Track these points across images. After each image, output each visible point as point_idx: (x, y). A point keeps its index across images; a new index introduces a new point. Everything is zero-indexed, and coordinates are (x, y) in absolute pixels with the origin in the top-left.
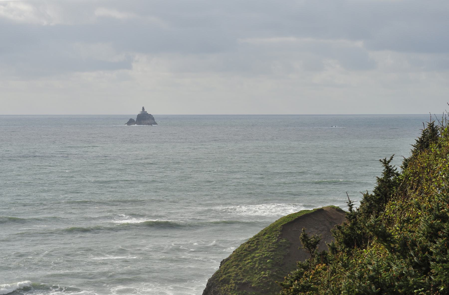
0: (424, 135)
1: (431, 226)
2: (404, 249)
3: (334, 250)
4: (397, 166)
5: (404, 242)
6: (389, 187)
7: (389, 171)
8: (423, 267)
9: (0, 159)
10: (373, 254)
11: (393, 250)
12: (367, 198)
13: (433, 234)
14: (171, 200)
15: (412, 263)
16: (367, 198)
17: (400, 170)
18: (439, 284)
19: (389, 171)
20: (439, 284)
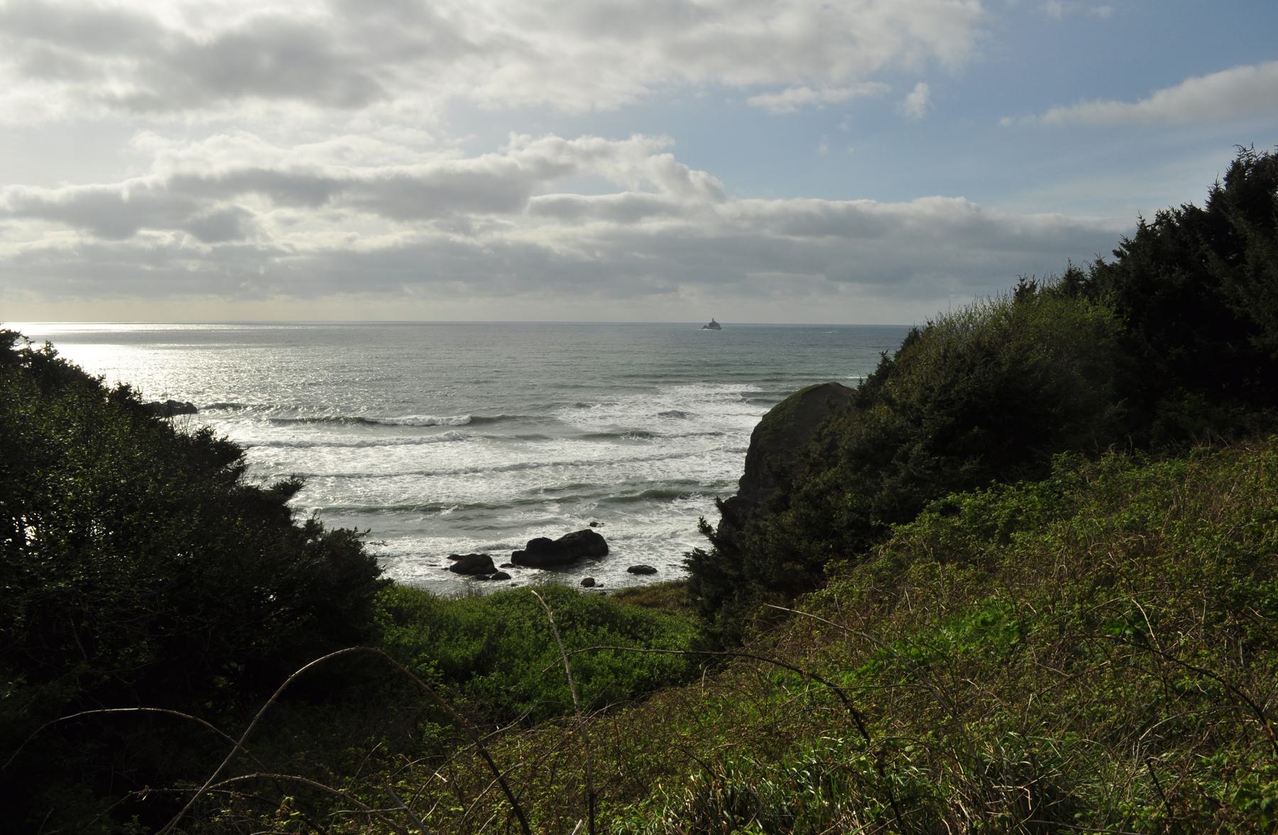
0: (929, 329)
1: (923, 395)
2: (904, 409)
3: (849, 409)
4: (891, 356)
5: (904, 406)
6: (886, 370)
7: (885, 360)
8: (917, 422)
9: (1277, 630)
10: (881, 412)
11: (895, 411)
12: (870, 376)
13: (924, 401)
14: (634, 541)
15: (909, 419)
16: (870, 376)
17: (892, 359)
18: (928, 433)
19: (885, 360)
20: (928, 433)
